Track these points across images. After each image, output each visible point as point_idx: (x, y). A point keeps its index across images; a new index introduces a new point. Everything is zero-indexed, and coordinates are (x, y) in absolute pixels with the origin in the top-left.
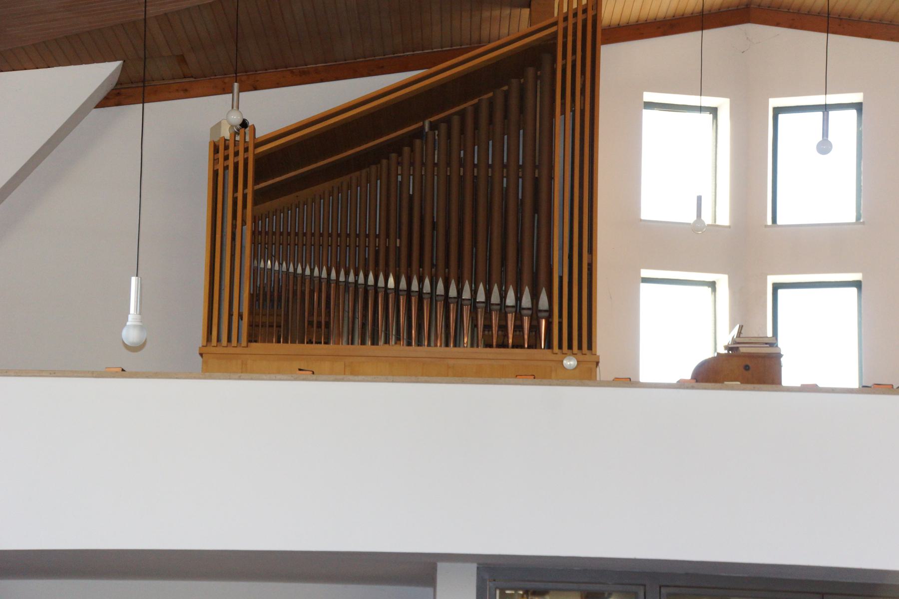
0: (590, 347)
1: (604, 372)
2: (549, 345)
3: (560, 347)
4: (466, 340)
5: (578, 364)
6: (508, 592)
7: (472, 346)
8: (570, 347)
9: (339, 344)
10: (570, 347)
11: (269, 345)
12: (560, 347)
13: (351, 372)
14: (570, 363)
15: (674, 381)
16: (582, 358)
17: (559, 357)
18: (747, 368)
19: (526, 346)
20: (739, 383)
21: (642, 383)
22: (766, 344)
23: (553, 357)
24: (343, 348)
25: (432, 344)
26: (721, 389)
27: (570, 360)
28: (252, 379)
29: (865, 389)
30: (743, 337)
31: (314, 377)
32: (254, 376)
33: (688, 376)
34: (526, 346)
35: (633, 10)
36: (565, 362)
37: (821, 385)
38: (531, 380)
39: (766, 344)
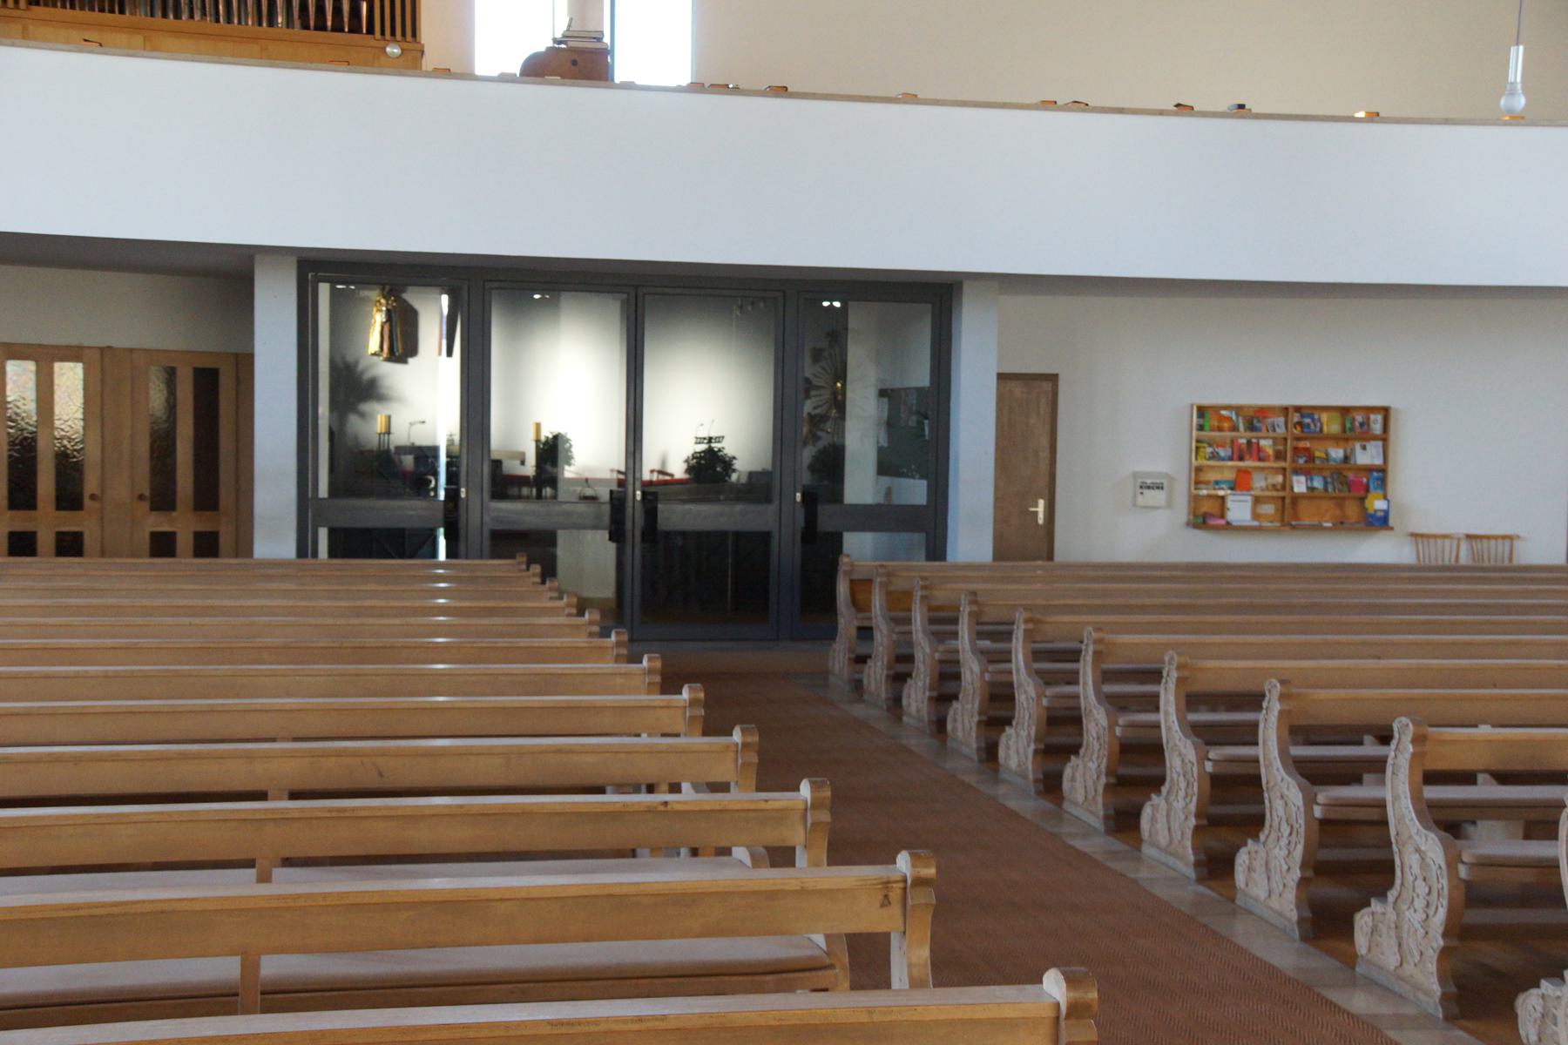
0: (414, 35)
1: (428, 63)
2: (370, 31)
3: (383, 33)
4: (280, 20)
5: (402, 53)
6: (339, 287)
7: (288, 27)
8: (393, 33)
9: (135, 15)
10: (393, 33)
11: (52, 10)
12: (383, 33)
13: (151, 47)
14: (393, 50)
15: (495, 74)
16: (405, 45)
17: (382, 43)
18: (574, 63)
19: (346, 30)
20: (559, 78)
21: (477, 76)
22: (594, 38)
23: (374, 43)
24: (141, 18)
25: (243, 23)
26: (540, 83)
27: (394, 48)
28: (366, 73)
29: (697, 87)
30: (623, 293)
31: (101, 49)
32: (243, 60)
33: (516, 69)
34: (346, 30)
35: (820, 973)
36: (388, 49)
37: (639, 82)
38: (344, 66)
39: (594, 38)
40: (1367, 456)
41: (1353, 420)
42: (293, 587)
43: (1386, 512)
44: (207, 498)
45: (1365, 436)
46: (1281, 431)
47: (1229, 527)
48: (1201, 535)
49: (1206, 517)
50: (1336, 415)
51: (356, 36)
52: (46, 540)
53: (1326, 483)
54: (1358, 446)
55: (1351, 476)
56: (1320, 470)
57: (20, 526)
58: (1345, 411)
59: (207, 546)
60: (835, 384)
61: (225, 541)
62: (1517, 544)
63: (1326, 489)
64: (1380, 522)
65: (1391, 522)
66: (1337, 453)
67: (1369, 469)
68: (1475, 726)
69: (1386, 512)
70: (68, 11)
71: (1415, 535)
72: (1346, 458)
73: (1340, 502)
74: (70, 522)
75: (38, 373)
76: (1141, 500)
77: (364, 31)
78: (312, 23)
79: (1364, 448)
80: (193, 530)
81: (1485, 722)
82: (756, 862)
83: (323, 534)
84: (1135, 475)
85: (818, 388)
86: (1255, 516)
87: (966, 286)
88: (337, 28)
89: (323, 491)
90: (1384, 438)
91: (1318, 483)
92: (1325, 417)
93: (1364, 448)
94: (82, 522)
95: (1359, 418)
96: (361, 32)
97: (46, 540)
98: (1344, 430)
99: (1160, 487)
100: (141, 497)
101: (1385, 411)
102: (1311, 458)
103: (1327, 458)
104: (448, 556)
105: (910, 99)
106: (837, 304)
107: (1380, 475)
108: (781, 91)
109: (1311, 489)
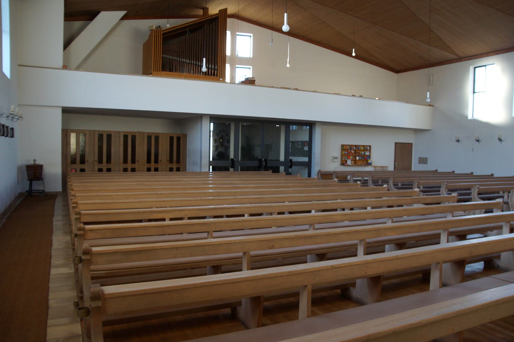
23: (218, 78)
40: (367, 153)
41: (365, 148)
42: (230, 174)
43: (371, 163)
44: (178, 161)
45: (367, 150)
46: (355, 149)
47: (348, 165)
48: (342, 167)
49: (344, 163)
50: (363, 147)
51: (214, 77)
52: (129, 169)
53: (361, 158)
54: (366, 152)
55: (365, 157)
56: (360, 156)
57: (149, 167)
58: (364, 146)
59: (178, 170)
60: (220, 140)
61: (181, 169)
62: (388, 168)
63: (361, 159)
64: (370, 164)
65: (372, 164)
66: (363, 153)
67: (367, 156)
68: (337, 200)
69: (371, 163)
70: (170, 72)
71: (374, 167)
72: (364, 154)
73: (363, 161)
74: (133, 166)
75: (77, 136)
76: (334, 161)
77: (216, 76)
78: (207, 74)
79: (367, 152)
80: (154, 167)
81: (339, 199)
82: (315, 212)
83: (211, 167)
84: (333, 157)
85: (217, 141)
86: (351, 163)
87: (316, 123)
88: (211, 75)
89: (211, 160)
90: (370, 151)
91: (360, 158)
92: (361, 147)
93: (367, 152)
94: (111, 166)
95: (366, 147)
96: (215, 76)
97: (105, 169)
98: (364, 149)
99: (337, 158)
100: (168, 161)
101: (370, 146)
102: (359, 154)
103: (362, 154)
104: (213, 170)
105: (315, 92)
106: (279, 126)
107: (369, 156)
108: (297, 89)
109: (359, 159)
